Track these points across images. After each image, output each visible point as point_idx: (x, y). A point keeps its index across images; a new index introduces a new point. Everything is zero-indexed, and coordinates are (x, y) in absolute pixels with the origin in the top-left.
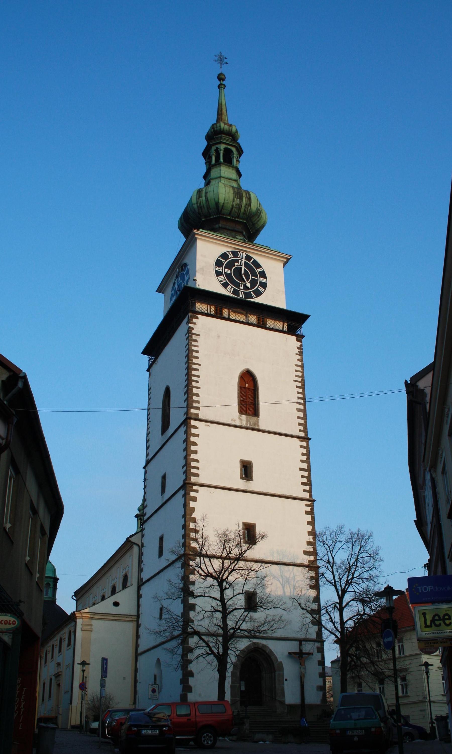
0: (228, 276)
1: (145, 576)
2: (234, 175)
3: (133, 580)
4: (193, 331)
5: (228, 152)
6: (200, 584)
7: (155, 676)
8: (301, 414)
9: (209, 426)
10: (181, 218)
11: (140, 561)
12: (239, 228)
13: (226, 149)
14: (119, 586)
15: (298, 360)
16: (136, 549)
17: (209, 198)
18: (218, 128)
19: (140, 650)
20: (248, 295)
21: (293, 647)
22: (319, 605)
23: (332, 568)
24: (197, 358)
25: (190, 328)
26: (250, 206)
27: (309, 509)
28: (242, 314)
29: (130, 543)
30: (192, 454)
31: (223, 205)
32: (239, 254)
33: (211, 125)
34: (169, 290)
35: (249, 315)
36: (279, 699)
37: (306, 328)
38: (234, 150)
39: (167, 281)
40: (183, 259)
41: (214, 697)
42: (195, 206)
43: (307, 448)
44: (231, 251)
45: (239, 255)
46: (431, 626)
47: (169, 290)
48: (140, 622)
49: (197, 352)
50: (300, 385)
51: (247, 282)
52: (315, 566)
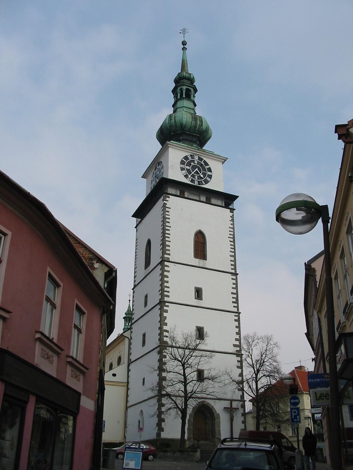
0: (188, 171)
1: (133, 358)
2: (192, 106)
3: (125, 360)
4: (167, 206)
5: (188, 91)
6: (171, 365)
7: (139, 421)
8: (233, 259)
9: (176, 265)
11: (130, 348)
12: (195, 139)
13: (187, 89)
14: (115, 364)
15: (231, 224)
16: (127, 340)
17: (176, 121)
18: (182, 76)
19: (128, 405)
21: (227, 404)
22: (243, 378)
23: (251, 356)
24: (169, 222)
25: (164, 203)
26: (202, 126)
27: (237, 318)
28: (197, 195)
29: (123, 337)
31: (185, 126)
32: (195, 157)
33: (178, 73)
34: (150, 177)
35: (201, 196)
36: (217, 437)
37: (236, 204)
38: (192, 90)
39: (148, 172)
40: (160, 158)
41: (178, 436)
42: (168, 125)
43: (236, 280)
44: (190, 155)
45: (195, 157)
46: (319, 400)
47: (150, 177)
48: (129, 387)
49: (169, 219)
50: (232, 240)
51: (201, 174)
52: (240, 354)
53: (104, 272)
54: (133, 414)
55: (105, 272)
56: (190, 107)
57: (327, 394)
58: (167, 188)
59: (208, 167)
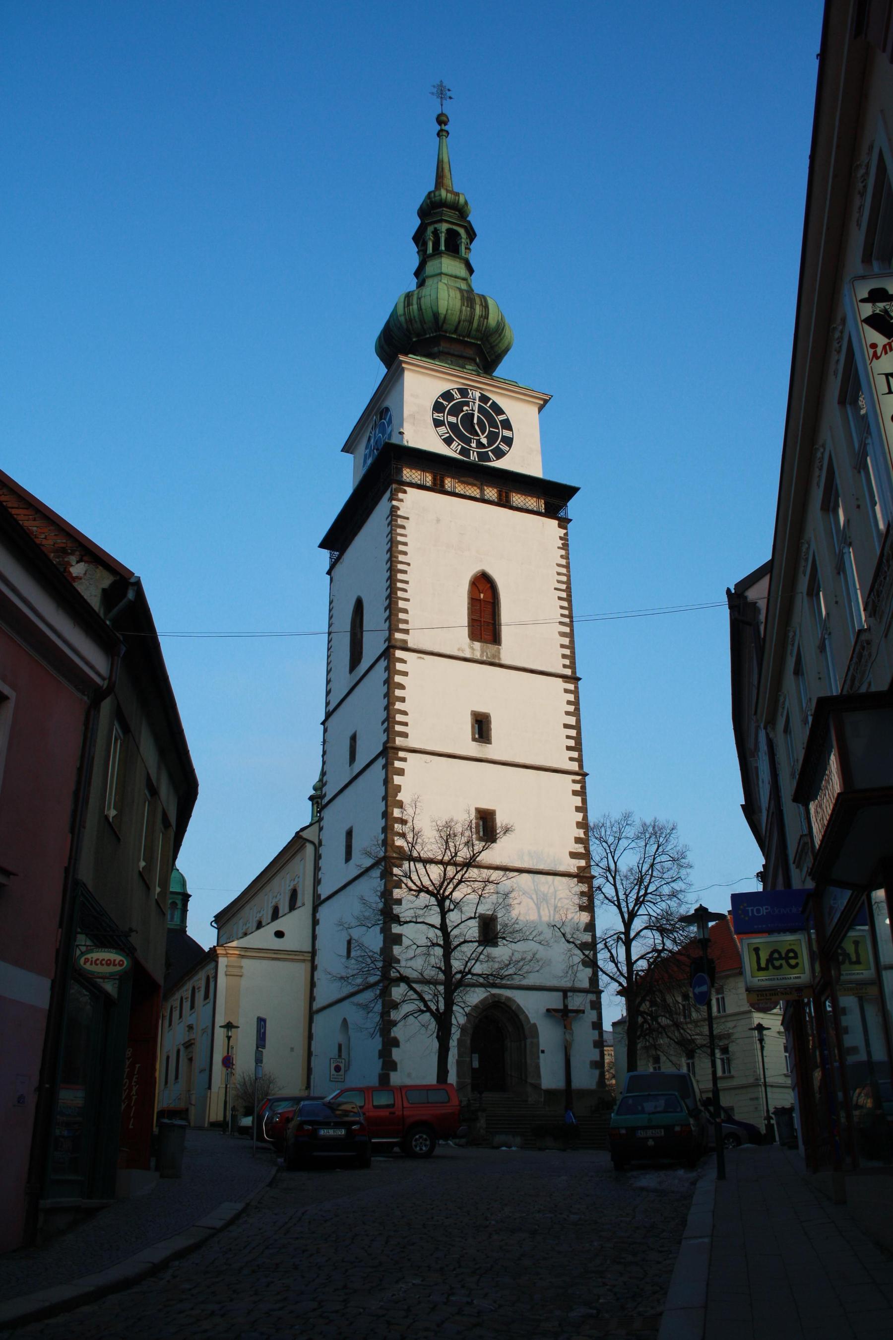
0: (453, 426)
2: (462, 272)
3: (306, 898)
4: (399, 513)
5: (452, 235)
6: (409, 903)
7: (340, 1046)
8: (566, 641)
10: (380, 337)
11: (317, 868)
12: (470, 352)
13: (449, 231)
14: (284, 907)
15: (562, 557)
16: (310, 848)
17: (423, 307)
19: (316, 1005)
20: (483, 457)
21: (554, 1001)
22: (594, 936)
23: (614, 878)
24: (405, 553)
25: (393, 507)
30: (397, 703)
33: (426, 193)
34: (362, 449)
36: (533, 1082)
37: (573, 507)
38: (462, 231)
40: (383, 401)
42: (402, 319)
43: (576, 692)
44: (458, 389)
46: (766, 969)
47: (362, 449)
49: (405, 544)
50: (564, 595)
51: (482, 437)
53: (100, 591)
54: (326, 1026)
55: (104, 590)
56: (458, 274)
57: (792, 951)
58: (400, 472)
59: (502, 417)
